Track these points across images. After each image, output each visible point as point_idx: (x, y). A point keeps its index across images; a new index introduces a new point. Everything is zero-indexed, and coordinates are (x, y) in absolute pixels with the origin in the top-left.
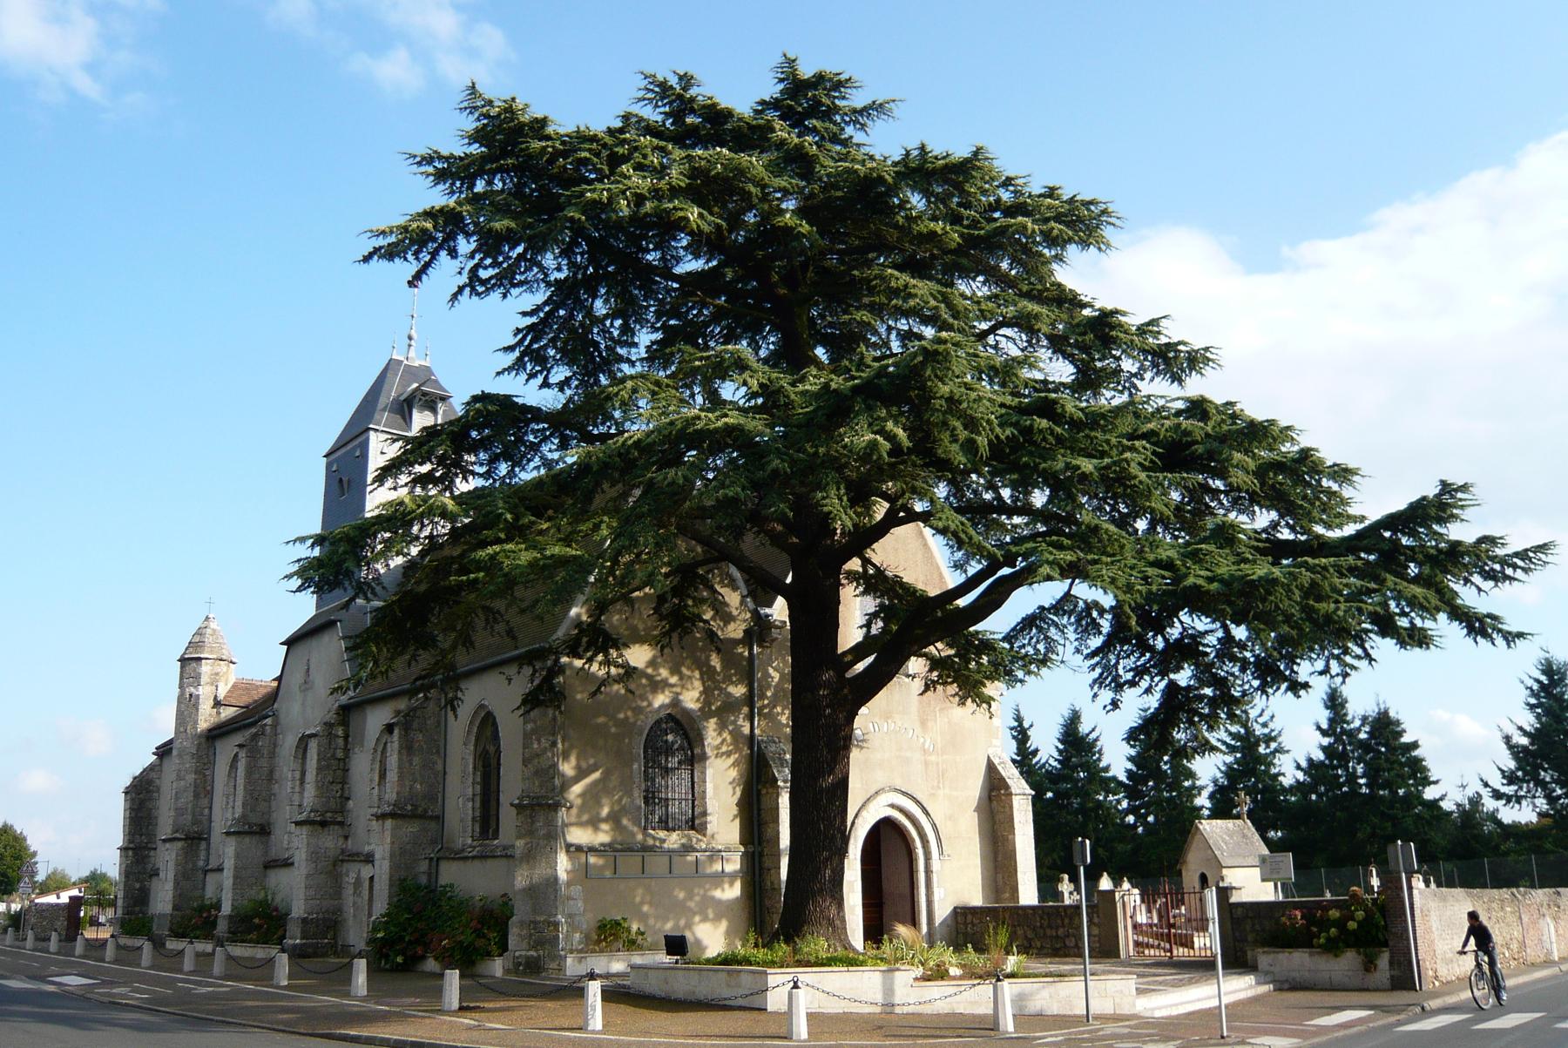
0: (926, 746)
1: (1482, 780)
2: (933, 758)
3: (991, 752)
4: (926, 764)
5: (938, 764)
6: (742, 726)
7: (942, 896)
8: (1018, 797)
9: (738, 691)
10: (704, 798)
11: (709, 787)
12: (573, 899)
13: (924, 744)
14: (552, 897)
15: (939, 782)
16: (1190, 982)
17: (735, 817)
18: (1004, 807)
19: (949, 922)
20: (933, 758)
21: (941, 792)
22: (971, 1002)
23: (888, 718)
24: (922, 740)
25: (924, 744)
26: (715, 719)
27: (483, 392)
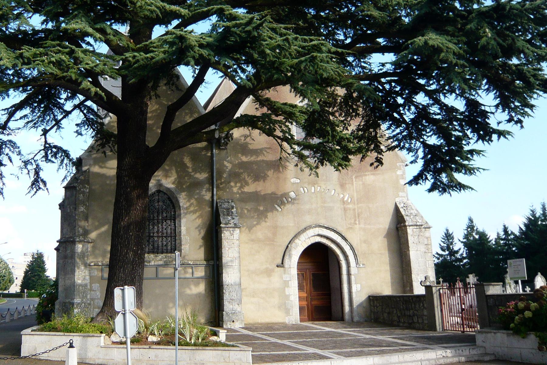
0: (345, 199)
1: (4, 198)
2: (351, 206)
3: (397, 200)
4: (345, 210)
5: (354, 210)
6: (204, 195)
7: (359, 289)
8: (411, 227)
9: (202, 176)
10: (180, 235)
11: (183, 229)
12: (94, 291)
13: (343, 198)
14: (73, 290)
15: (355, 220)
16: (416, 349)
17: (201, 246)
18: (404, 234)
19: (365, 305)
20: (351, 206)
21: (357, 226)
22: (137, 360)
23: (315, 184)
24: (342, 196)
25: (343, 198)
26: (185, 193)
27: (160, 26)
